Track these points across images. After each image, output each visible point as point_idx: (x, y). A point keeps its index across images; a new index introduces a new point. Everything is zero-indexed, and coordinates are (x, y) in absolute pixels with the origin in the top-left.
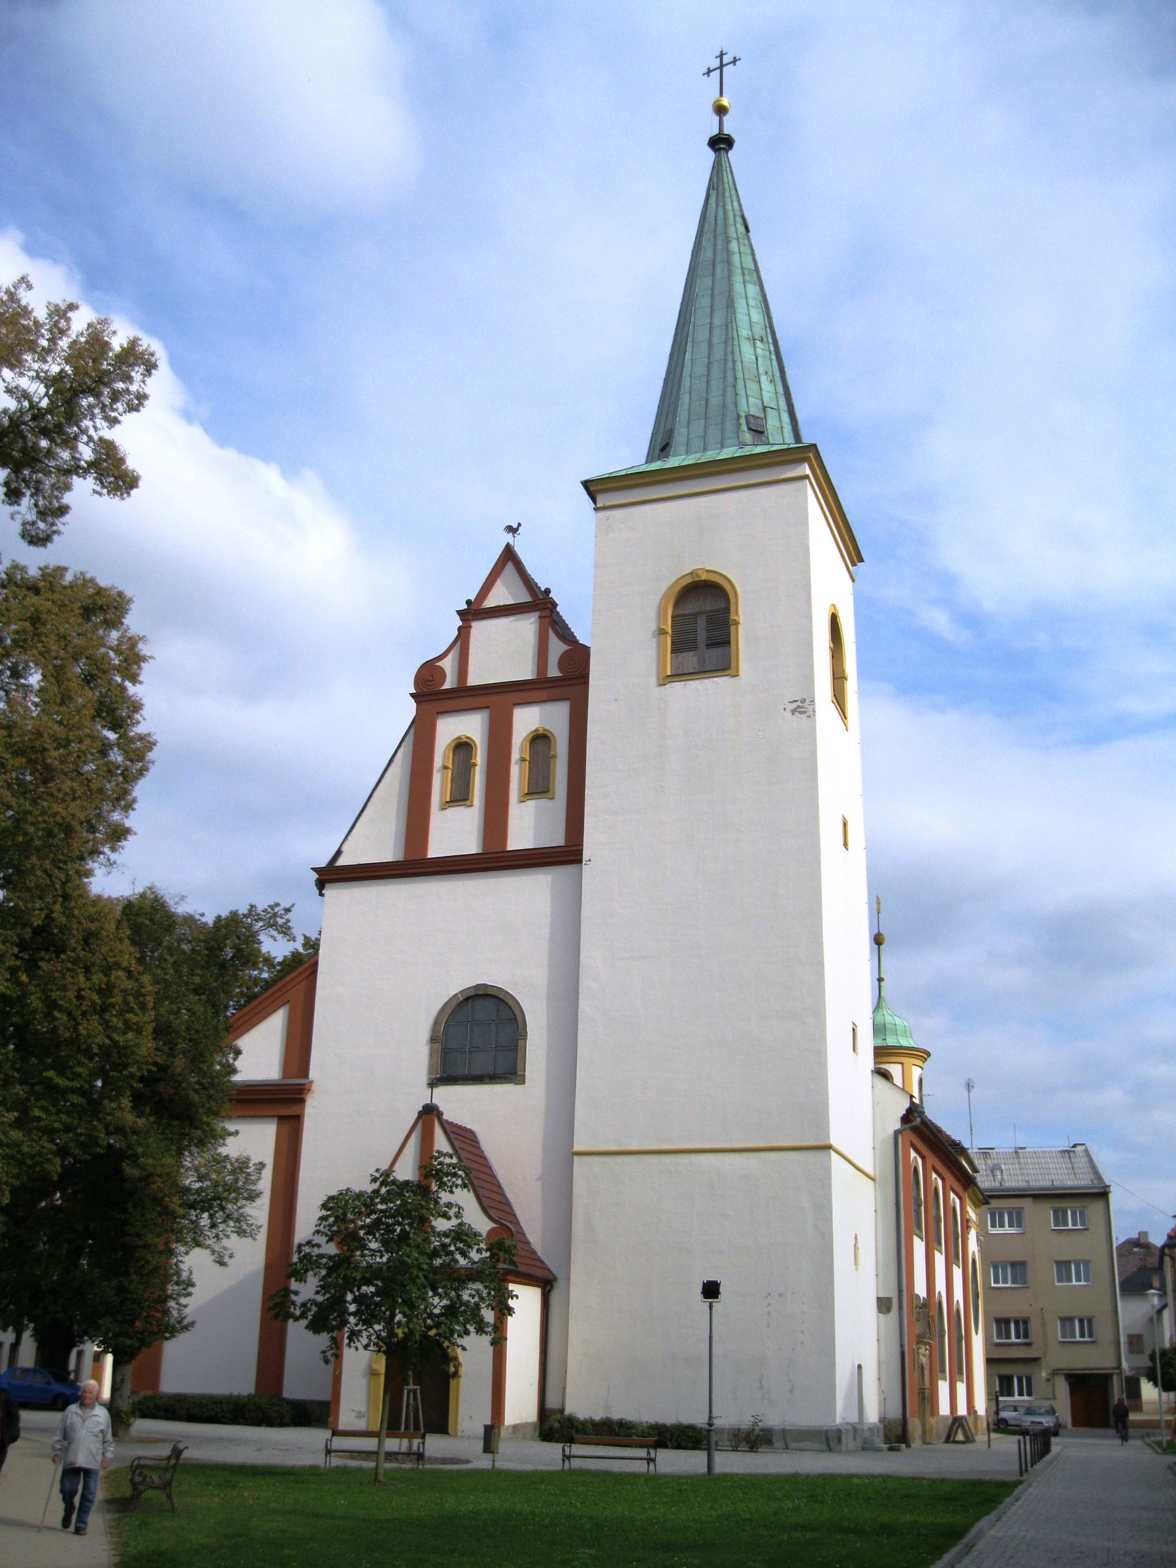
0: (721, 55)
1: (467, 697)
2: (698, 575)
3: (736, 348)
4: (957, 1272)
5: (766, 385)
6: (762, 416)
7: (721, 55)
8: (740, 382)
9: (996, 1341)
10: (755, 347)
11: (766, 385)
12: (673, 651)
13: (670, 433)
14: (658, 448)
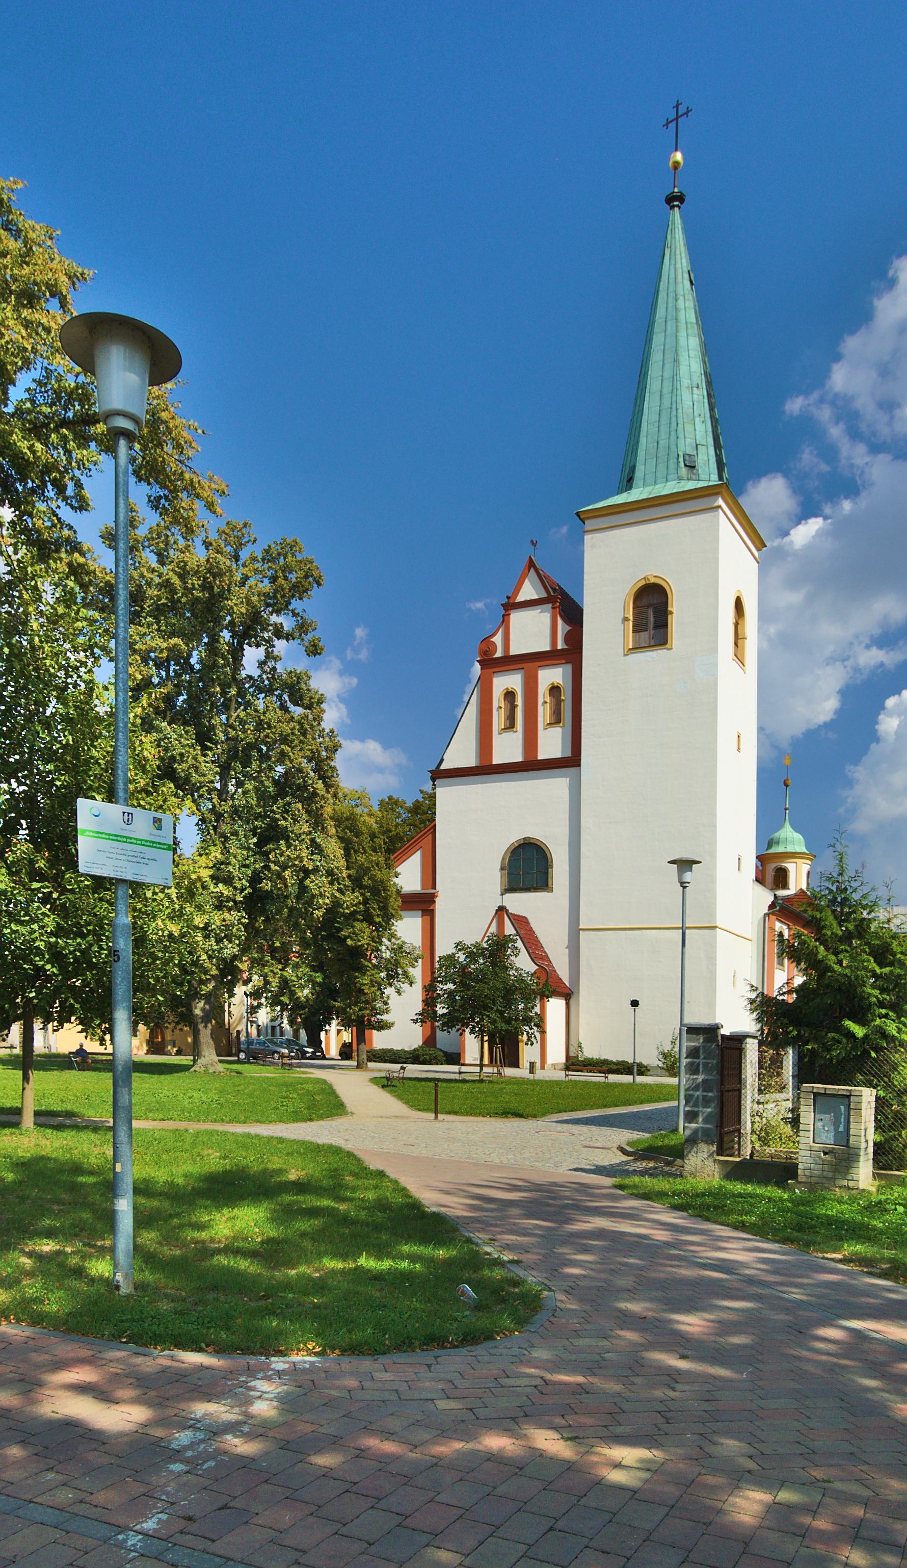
0: (677, 107)
1: (511, 662)
3: (679, 397)
5: (700, 427)
7: (677, 107)
11: (700, 427)
12: (634, 631)
13: (633, 469)
14: (626, 479)
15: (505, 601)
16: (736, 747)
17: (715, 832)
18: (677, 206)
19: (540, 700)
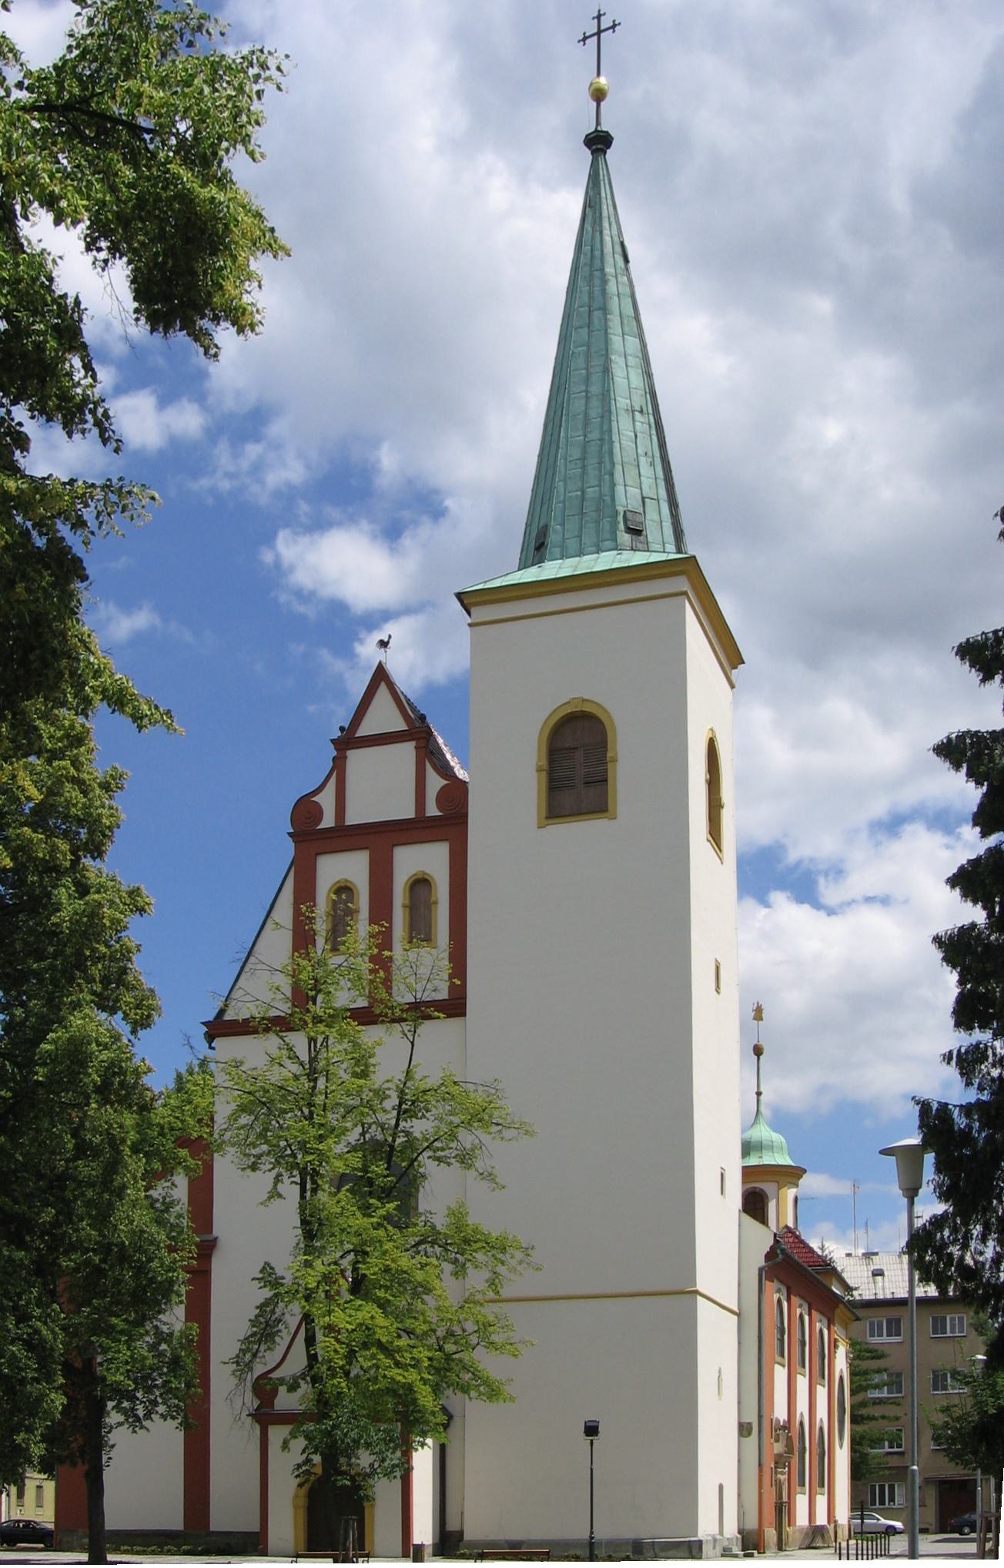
0: (599, 17)
1: (347, 837)
3: (614, 424)
4: (822, 1393)
5: (646, 470)
7: (599, 17)
8: (618, 468)
10: (634, 421)
11: (646, 470)
13: (543, 532)
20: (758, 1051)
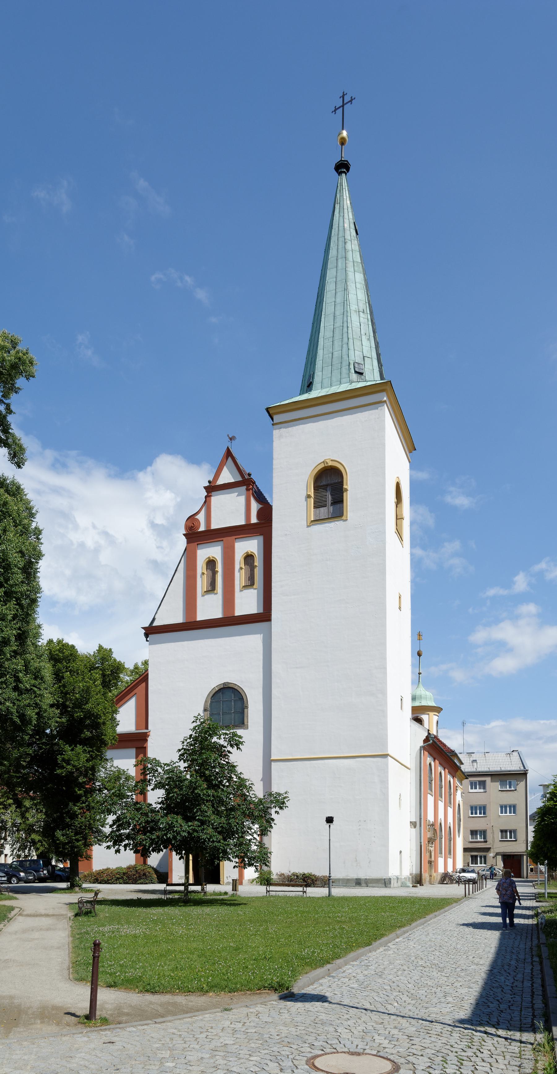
1: (213, 535)
2: (327, 463)
3: (349, 318)
4: (450, 811)
6: (363, 363)
8: (351, 341)
9: (471, 840)
12: (315, 507)
13: (312, 376)
14: (306, 385)
15: (207, 484)
16: (402, 598)
17: (385, 673)
18: (344, 172)
19: (237, 567)
20: (419, 654)
